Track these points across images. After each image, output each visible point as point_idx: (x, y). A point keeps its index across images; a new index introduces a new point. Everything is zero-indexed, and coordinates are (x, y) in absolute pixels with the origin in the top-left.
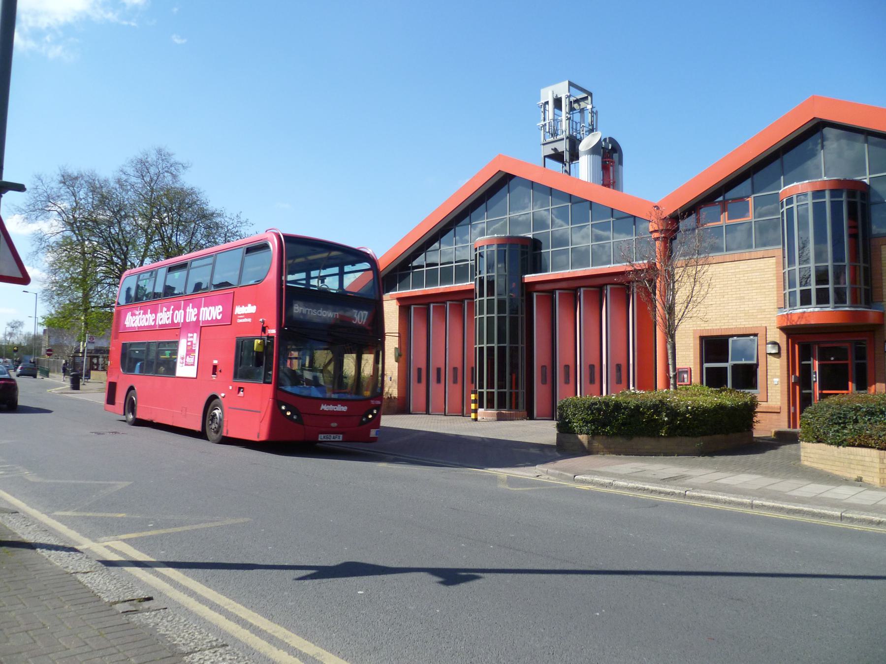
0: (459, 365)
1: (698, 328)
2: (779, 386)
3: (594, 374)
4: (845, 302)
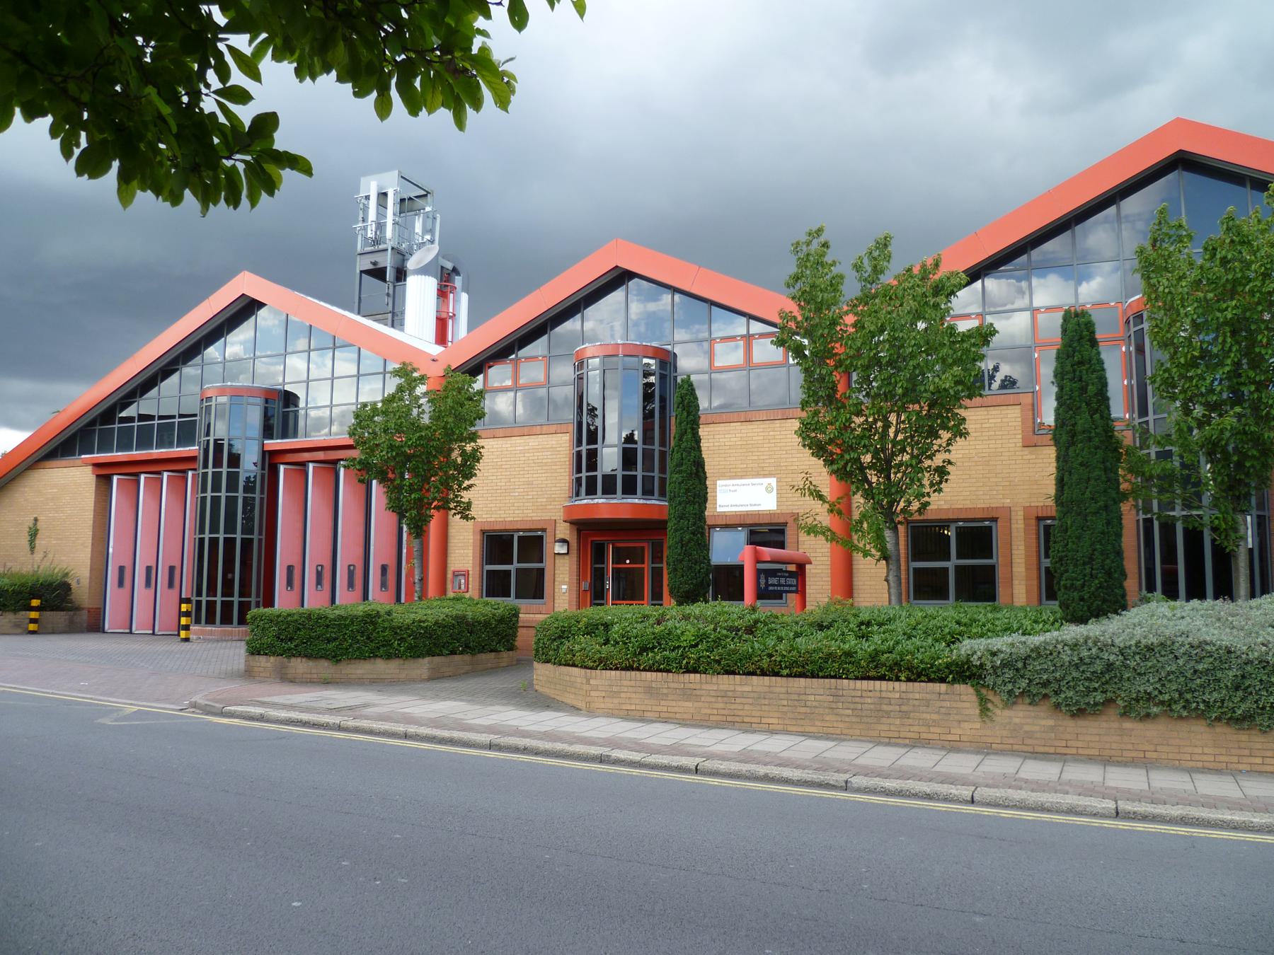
0: (127, 564)
2: (567, 594)
3: (327, 576)
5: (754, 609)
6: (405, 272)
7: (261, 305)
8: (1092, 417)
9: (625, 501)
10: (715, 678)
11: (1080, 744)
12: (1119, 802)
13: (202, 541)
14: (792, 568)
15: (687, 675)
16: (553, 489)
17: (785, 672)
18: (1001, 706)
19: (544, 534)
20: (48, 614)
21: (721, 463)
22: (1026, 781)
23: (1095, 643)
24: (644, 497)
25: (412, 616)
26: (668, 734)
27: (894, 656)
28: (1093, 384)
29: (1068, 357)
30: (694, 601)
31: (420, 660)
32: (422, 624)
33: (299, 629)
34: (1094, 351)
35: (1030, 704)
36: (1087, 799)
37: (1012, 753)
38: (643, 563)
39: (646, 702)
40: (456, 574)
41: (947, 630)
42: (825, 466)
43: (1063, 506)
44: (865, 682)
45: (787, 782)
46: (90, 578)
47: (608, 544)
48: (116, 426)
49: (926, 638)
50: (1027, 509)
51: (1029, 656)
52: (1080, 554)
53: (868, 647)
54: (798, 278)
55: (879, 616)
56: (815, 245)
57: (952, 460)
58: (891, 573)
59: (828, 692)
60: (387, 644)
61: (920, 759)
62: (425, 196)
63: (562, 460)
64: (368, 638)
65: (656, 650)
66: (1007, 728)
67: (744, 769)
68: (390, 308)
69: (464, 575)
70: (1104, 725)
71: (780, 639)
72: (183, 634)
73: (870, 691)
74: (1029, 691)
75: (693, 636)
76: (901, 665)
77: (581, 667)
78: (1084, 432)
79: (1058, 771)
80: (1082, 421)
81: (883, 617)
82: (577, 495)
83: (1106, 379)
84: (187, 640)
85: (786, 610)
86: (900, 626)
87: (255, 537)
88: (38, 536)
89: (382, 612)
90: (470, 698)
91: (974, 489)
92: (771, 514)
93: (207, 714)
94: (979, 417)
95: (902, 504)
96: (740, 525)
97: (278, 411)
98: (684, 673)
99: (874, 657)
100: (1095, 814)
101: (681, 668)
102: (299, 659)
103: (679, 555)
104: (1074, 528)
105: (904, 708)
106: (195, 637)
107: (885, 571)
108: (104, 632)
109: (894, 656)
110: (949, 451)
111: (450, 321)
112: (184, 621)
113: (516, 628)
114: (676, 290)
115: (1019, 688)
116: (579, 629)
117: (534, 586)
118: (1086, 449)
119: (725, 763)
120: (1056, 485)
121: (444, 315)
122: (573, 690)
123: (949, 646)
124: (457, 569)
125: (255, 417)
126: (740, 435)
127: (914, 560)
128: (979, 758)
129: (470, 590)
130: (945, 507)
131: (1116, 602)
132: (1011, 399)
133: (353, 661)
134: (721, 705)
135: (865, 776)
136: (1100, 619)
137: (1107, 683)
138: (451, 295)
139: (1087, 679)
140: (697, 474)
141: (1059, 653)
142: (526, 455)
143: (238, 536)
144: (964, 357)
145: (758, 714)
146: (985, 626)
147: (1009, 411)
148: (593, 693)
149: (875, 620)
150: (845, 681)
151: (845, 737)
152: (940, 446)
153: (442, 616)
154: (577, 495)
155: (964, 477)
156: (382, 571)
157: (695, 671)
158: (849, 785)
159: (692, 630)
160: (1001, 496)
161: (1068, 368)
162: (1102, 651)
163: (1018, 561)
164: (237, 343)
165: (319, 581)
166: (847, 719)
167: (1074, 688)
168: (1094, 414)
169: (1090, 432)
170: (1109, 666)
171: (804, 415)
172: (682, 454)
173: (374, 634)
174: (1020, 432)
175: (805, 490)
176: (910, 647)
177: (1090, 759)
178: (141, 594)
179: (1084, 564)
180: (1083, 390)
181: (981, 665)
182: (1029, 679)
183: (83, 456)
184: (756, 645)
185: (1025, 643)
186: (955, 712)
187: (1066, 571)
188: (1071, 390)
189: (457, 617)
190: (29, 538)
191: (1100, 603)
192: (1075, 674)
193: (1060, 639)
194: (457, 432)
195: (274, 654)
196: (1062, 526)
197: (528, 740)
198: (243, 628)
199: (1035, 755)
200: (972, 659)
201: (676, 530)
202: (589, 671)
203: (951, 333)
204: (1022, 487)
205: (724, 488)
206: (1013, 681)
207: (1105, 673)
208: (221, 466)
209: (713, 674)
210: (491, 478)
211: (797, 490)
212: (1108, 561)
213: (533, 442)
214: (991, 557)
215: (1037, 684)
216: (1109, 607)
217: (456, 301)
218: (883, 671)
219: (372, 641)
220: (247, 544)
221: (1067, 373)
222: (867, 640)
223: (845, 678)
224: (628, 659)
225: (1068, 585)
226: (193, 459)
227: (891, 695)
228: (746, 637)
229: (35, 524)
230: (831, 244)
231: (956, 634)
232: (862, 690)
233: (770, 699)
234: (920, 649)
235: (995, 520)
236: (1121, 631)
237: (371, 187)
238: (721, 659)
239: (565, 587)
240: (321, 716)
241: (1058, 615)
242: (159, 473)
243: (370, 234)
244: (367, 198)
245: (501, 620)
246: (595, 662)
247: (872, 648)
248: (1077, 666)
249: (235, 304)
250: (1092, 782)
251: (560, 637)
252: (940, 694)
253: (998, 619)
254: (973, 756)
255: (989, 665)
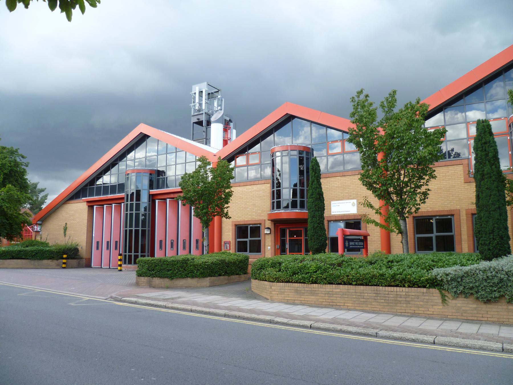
0: (163, 239)
1: (234, 220)
2: (270, 250)
3: (187, 245)
4: (296, 207)
5: (343, 256)
6: (210, 122)
7: (148, 137)
8: (491, 167)
9: (292, 211)
10: (324, 286)
11: (489, 316)
12: (504, 344)
13: (126, 231)
14: (362, 238)
15: (312, 285)
16: (264, 207)
17: (354, 283)
18: (452, 298)
19: (260, 226)
20: (70, 261)
21: (333, 194)
22: (461, 334)
23: (494, 270)
24: (300, 209)
25: (202, 260)
26: (303, 311)
27: (402, 276)
28: (491, 152)
29: (479, 141)
30: (320, 252)
31: (206, 279)
32: (206, 263)
33: (156, 266)
34: (491, 137)
35: (465, 297)
36: (489, 342)
37: (456, 320)
38: (301, 237)
39: (295, 296)
40: (225, 243)
41: (427, 264)
42: (373, 193)
43: (479, 208)
44: (390, 288)
45: (350, 333)
46: (86, 246)
47: (287, 229)
48: (95, 186)
49: (418, 268)
50: (467, 210)
51: (464, 276)
52: (487, 229)
53: (391, 272)
54: (355, 114)
55: (397, 258)
56: (362, 97)
57: (429, 189)
58: (404, 239)
59: (373, 292)
60: (192, 272)
61: (413, 323)
62: (218, 91)
63: (267, 195)
64: (184, 269)
65: (299, 274)
66: (455, 308)
67: (331, 327)
68: (205, 137)
69: (228, 243)
70: (500, 307)
71: (352, 269)
72: (119, 268)
73: (392, 292)
74: (464, 291)
75: (315, 268)
76: (405, 280)
77: (268, 281)
78: (488, 174)
79: (477, 329)
80: (487, 169)
81: (399, 259)
82: (273, 209)
83: (497, 150)
84: (121, 270)
85: (357, 257)
86: (406, 262)
87: (147, 229)
88: (67, 230)
89: (190, 259)
90: (223, 294)
91: (443, 202)
92: (354, 215)
93: (115, 301)
94: (444, 171)
95: (407, 210)
96: (341, 220)
97: (155, 178)
98: (311, 284)
99: (393, 276)
100: (492, 350)
101: (310, 282)
102: (157, 278)
103: (313, 233)
104: (484, 217)
105: (408, 299)
106: (124, 269)
107: (401, 238)
108: (91, 267)
109: (402, 276)
110: (427, 185)
111: (229, 141)
112: (119, 263)
113: (248, 265)
114: (312, 122)
115: (459, 290)
116: (269, 265)
117: (257, 247)
118: (489, 181)
119: (323, 324)
120: (476, 198)
121: (226, 139)
122: (265, 291)
123: (428, 271)
124: (226, 241)
125: (146, 182)
126: (340, 182)
127: (417, 233)
128: (441, 322)
129: (231, 249)
130: (430, 210)
131: (505, 250)
132: (458, 162)
133: (178, 279)
134: (327, 298)
135: (386, 331)
136: (498, 258)
137: (500, 288)
138: (229, 131)
139: (491, 286)
140: (320, 198)
141: (477, 274)
142: (253, 193)
143: (140, 229)
144: (432, 143)
145: (343, 302)
146: (445, 262)
147: (457, 168)
148: (273, 293)
149: (395, 260)
150: (381, 287)
151: (381, 312)
152: (424, 183)
153: (215, 260)
154: (273, 209)
155: (438, 197)
156: (196, 242)
157: (316, 283)
158: (378, 335)
159: (314, 265)
160: (455, 205)
161: (480, 146)
162: (498, 273)
163: (464, 233)
164: (139, 154)
165: (172, 246)
166: (382, 304)
167: (485, 290)
168: (492, 166)
169: (490, 174)
170: (501, 280)
171: (362, 172)
172: (313, 190)
173: (187, 268)
174: (463, 176)
175: (365, 204)
176: (410, 272)
177: (493, 323)
178: (105, 251)
179: (490, 233)
180: (487, 155)
181: (442, 280)
182: (464, 286)
183: (83, 198)
184: (342, 271)
185: (461, 269)
186: (431, 301)
187: (482, 237)
188: (481, 155)
189: (221, 260)
190: (63, 231)
191: (498, 251)
192: (485, 284)
193: (478, 268)
194: (221, 184)
195: (147, 276)
196: (479, 217)
197: (241, 313)
198: (136, 266)
199: (468, 321)
200: (437, 277)
201: (311, 223)
202: (271, 283)
203: (425, 133)
204: (464, 201)
205: (334, 204)
206: (456, 287)
207: (499, 283)
208: (133, 201)
209: (323, 284)
210: (238, 203)
211: (361, 205)
212: (501, 232)
213: (255, 187)
214: (452, 232)
215: (468, 288)
216: (502, 253)
217: (231, 133)
218: (397, 283)
219: (186, 271)
220: (144, 232)
221: (479, 148)
222: (390, 269)
223: (381, 286)
224: (287, 278)
225: (483, 243)
226: (123, 198)
227: (401, 293)
228: (337, 268)
229: (66, 225)
230: (369, 95)
231: (432, 266)
232: (388, 291)
233: (348, 295)
234: (414, 273)
235: (453, 215)
236: (506, 264)
237: (196, 89)
238: (327, 278)
239: (269, 247)
240: (159, 302)
241: (480, 257)
242: (111, 204)
243: (197, 108)
244: (195, 93)
245: (241, 261)
246: (274, 279)
247: (393, 272)
248: (486, 280)
249: (138, 137)
250: (493, 334)
251: (261, 269)
252: (423, 293)
253: (451, 259)
254: (439, 321)
255: (445, 280)
